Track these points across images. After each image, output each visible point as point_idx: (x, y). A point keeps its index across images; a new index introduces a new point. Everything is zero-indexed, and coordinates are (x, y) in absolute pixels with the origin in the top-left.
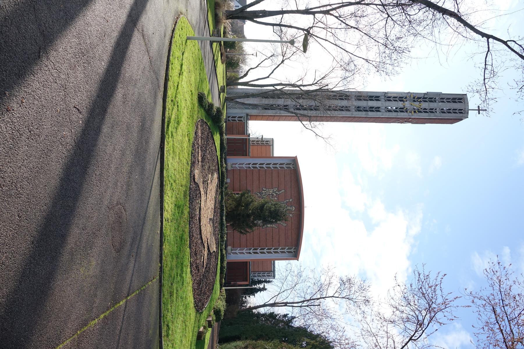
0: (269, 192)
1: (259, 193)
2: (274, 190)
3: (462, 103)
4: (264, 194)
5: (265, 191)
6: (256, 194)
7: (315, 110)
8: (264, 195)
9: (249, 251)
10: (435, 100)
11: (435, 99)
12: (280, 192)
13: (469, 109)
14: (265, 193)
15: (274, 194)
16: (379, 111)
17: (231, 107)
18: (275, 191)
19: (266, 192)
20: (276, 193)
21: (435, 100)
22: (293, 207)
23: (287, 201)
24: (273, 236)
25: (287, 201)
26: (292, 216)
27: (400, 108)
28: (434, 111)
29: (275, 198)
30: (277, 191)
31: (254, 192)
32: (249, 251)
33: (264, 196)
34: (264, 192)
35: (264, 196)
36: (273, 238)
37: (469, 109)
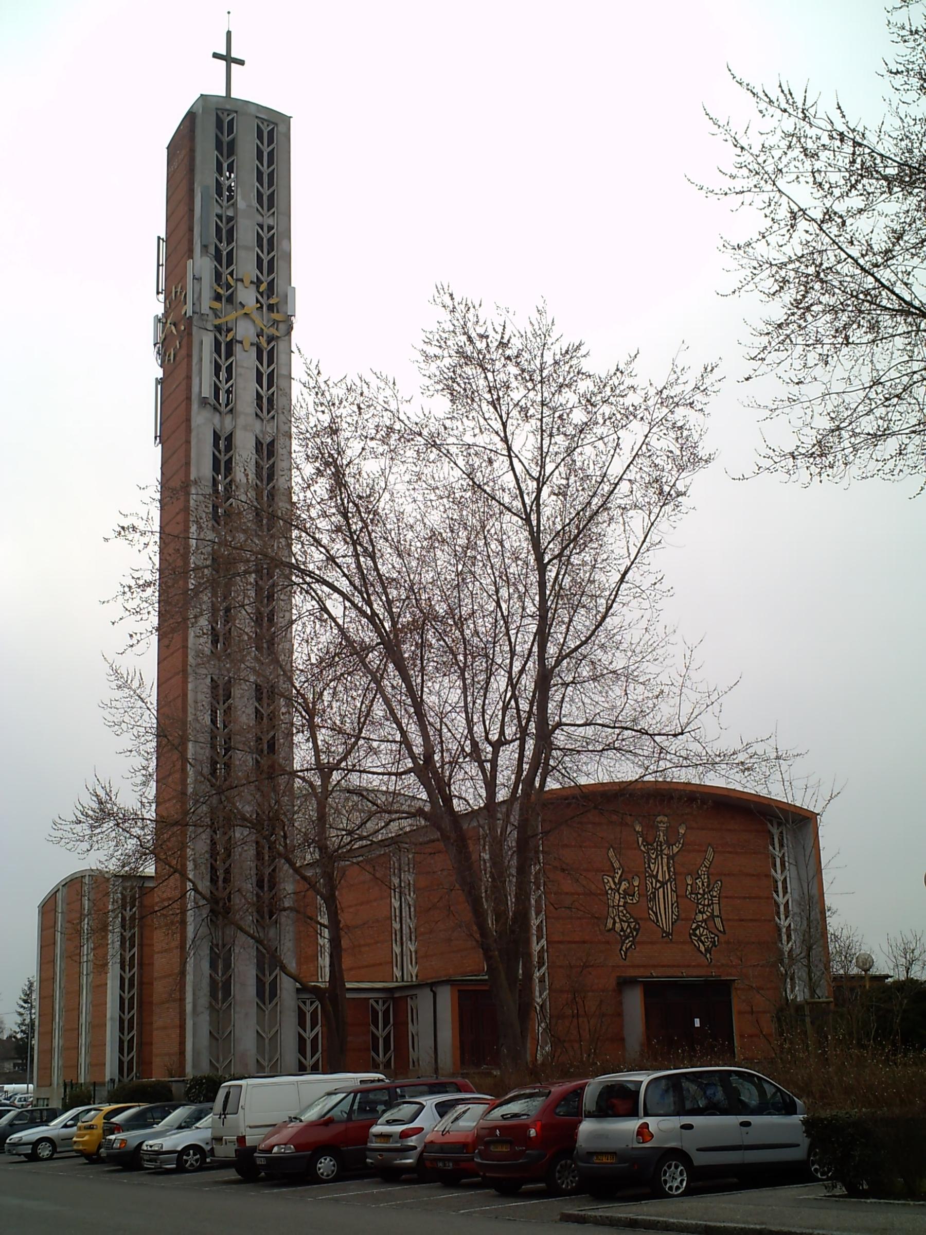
0: (619, 906)
1: (623, 943)
2: (611, 888)
3: (233, 119)
4: (625, 925)
5: (614, 923)
6: (626, 953)
7: (229, 697)
8: (629, 926)
9: (267, 1041)
10: (265, 229)
11: (219, 217)
12: (616, 865)
13: (224, 94)
14: (621, 920)
15: (623, 887)
16: (230, 438)
17: (270, 1061)
18: (614, 882)
19: (617, 918)
20: (620, 883)
21: (265, 229)
22: (659, 819)
23: (640, 839)
24: (745, 898)
25: (640, 839)
26: (683, 826)
27: (260, 358)
28: (265, 236)
29: (636, 884)
30: (613, 878)
31: (622, 963)
32: (267, 1041)
33: (632, 925)
34: (618, 925)
35: (632, 925)
36: (749, 898)
37: (224, 94)
